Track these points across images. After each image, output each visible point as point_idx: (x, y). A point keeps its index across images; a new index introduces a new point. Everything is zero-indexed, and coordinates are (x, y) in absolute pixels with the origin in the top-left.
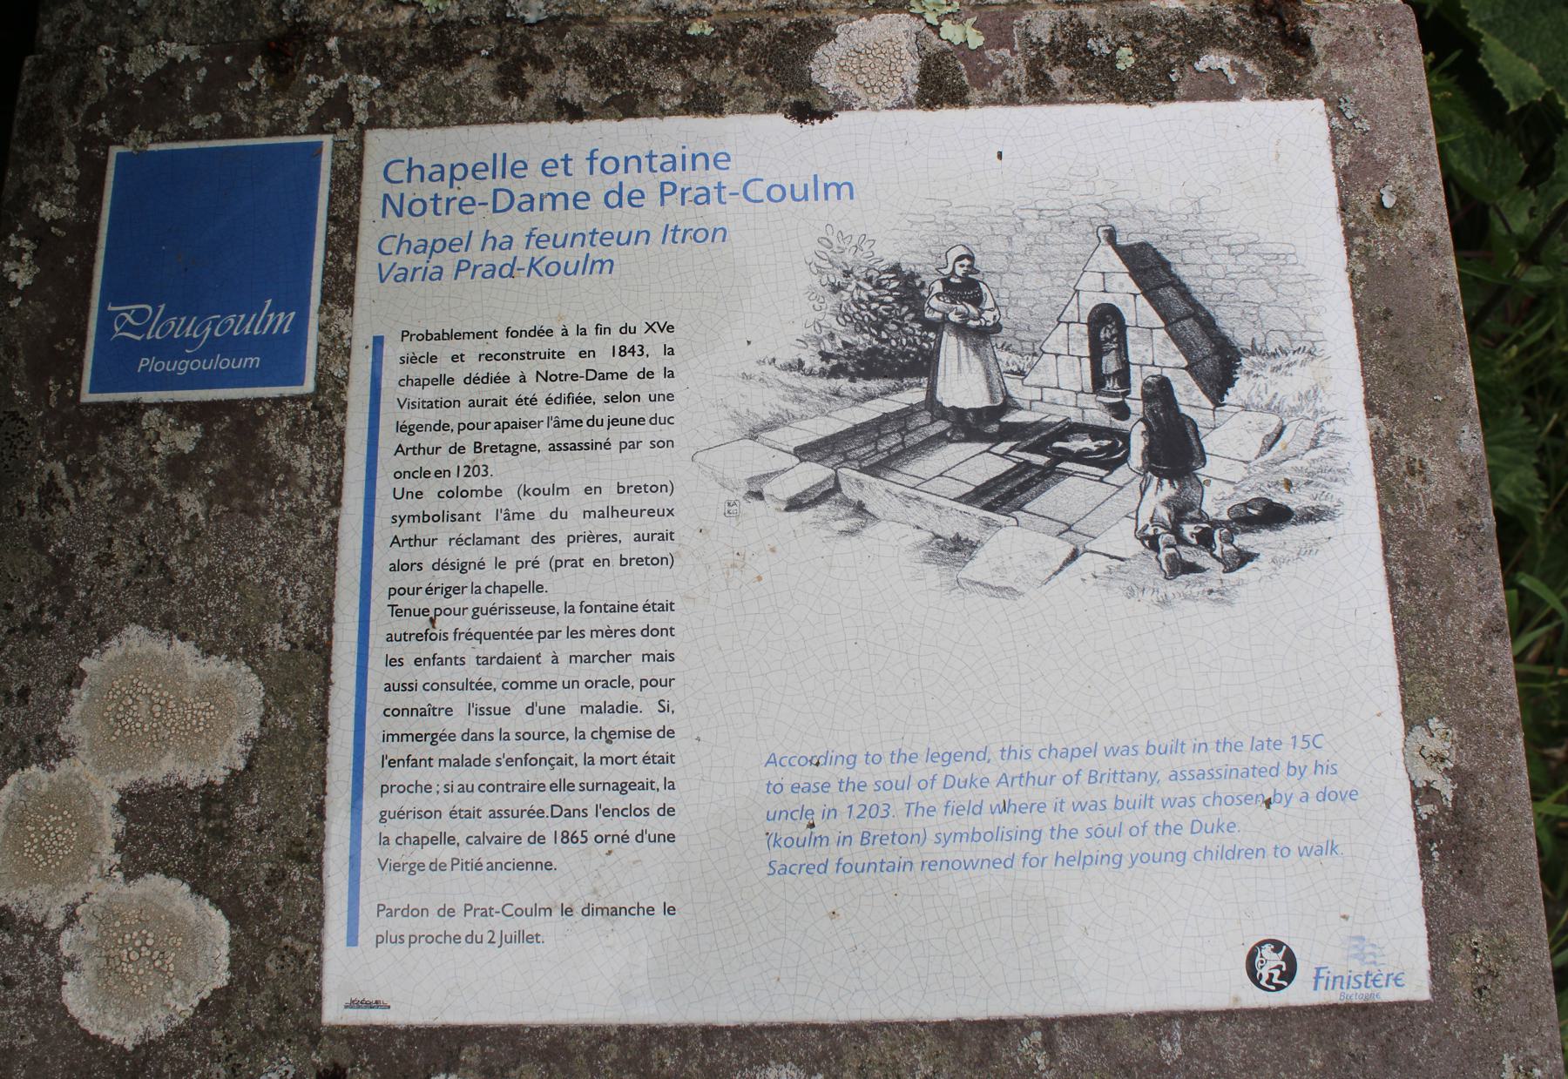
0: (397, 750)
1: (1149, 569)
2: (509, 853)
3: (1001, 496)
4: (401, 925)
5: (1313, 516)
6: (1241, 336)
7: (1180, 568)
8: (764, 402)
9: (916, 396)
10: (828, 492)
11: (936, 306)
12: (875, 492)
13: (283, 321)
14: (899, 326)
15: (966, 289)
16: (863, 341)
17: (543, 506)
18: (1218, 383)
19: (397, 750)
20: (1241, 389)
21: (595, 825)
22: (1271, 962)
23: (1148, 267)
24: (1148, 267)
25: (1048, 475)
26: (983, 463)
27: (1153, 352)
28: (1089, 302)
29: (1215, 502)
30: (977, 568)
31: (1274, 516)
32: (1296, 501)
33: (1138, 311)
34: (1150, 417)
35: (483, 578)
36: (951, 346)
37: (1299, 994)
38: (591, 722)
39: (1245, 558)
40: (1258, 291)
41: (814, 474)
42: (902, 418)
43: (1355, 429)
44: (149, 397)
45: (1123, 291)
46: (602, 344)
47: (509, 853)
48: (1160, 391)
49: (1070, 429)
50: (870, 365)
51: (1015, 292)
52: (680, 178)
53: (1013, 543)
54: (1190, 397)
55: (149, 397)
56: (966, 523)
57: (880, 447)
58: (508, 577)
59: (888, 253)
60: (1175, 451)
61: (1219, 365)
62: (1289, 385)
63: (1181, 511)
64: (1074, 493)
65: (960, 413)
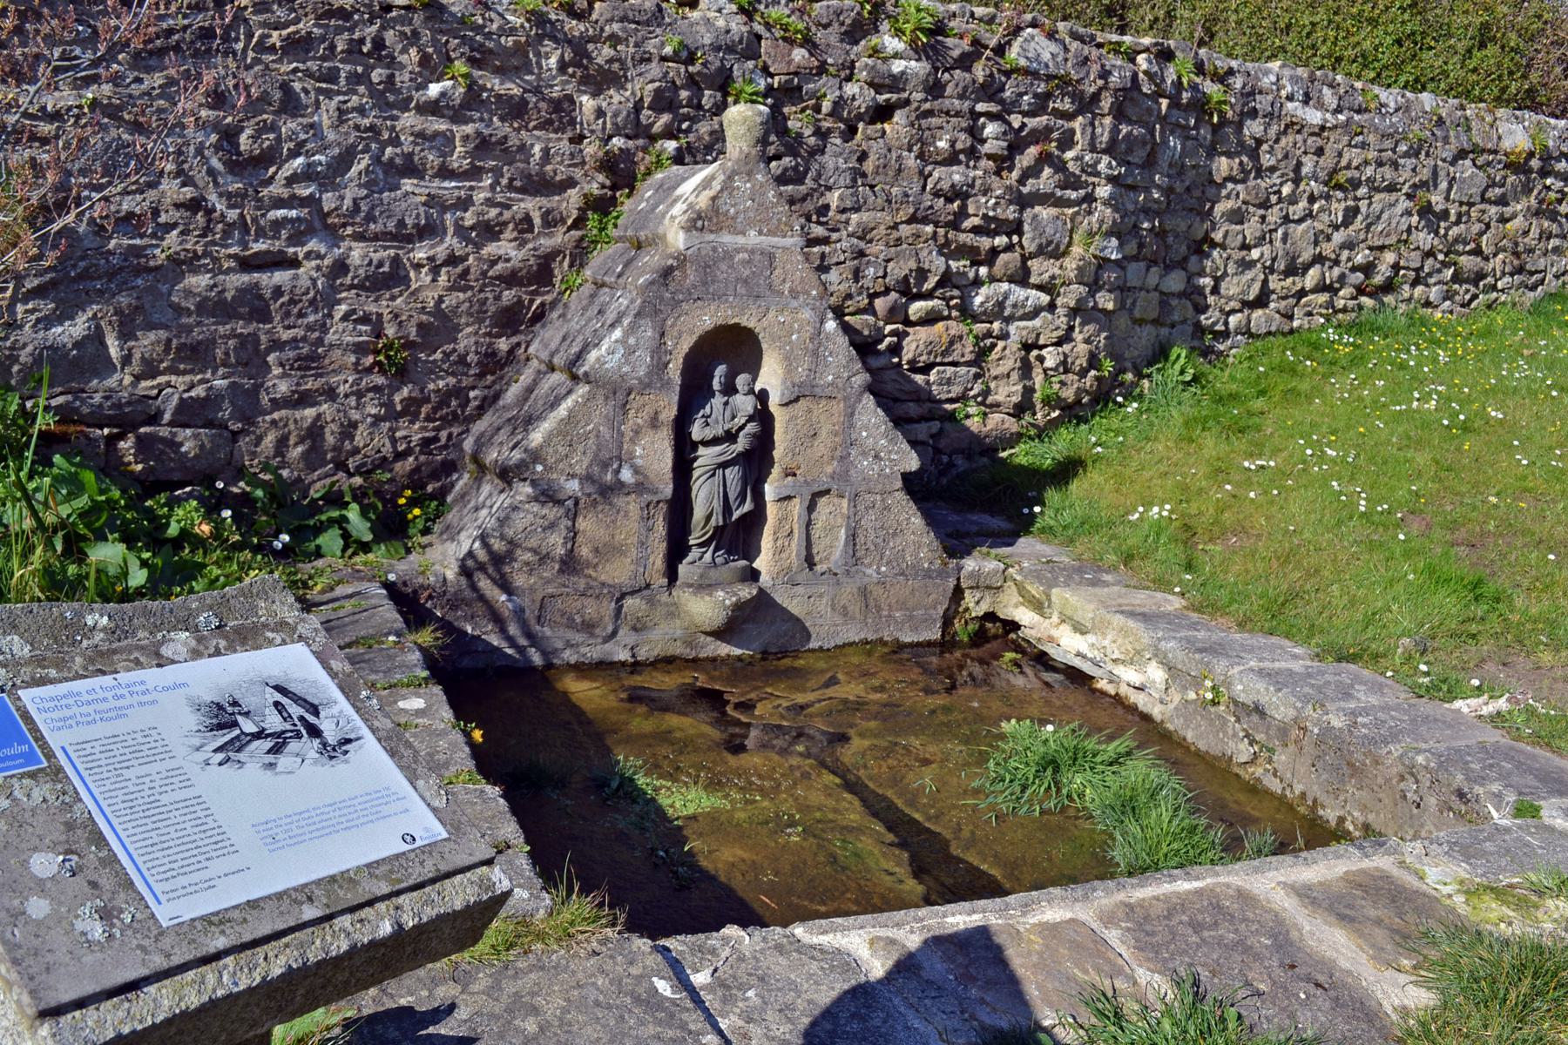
0: (150, 865)
1: (325, 759)
2: (192, 868)
3: (276, 750)
4: (171, 895)
5: (358, 739)
6: (316, 702)
7: (332, 758)
8: (197, 742)
9: (237, 732)
10: (228, 760)
11: (230, 710)
12: (241, 756)
13: (25, 748)
14: (222, 716)
15: (235, 704)
16: (215, 721)
17: (147, 780)
18: (316, 713)
19: (150, 865)
20: (322, 714)
21: (214, 854)
22: (408, 839)
23: (279, 689)
24: (279, 689)
25: (284, 743)
26: (268, 744)
27: (295, 710)
28: (271, 701)
29: (332, 740)
30: (279, 769)
31: (348, 741)
32: (352, 736)
33: (284, 701)
34: (302, 722)
35: (141, 801)
36: (239, 718)
37: (419, 843)
38: (196, 830)
39: (346, 752)
40: (313, 690)
41: (220, 756)
42: (237, 737)
43: (355, 716)
44: (13, 709)
45: (278, 697)
46: (138, 736)
47: (192, 868)
48: (302, 718)
49: (284, 732)
50: (220, 727)
51: (248, 702)
52: (135, 689)
53: (284, 761)
54: (311, 719)
55: (13, 709)
56: (271, 758)
57: (238, 744)
58: (147, 800)
59: (208, 698)
60: (314, 732)
61: (315, 711)
62: (335, 710)
63: (325, 745)
64: (293, 746)
65: (252, 734)
